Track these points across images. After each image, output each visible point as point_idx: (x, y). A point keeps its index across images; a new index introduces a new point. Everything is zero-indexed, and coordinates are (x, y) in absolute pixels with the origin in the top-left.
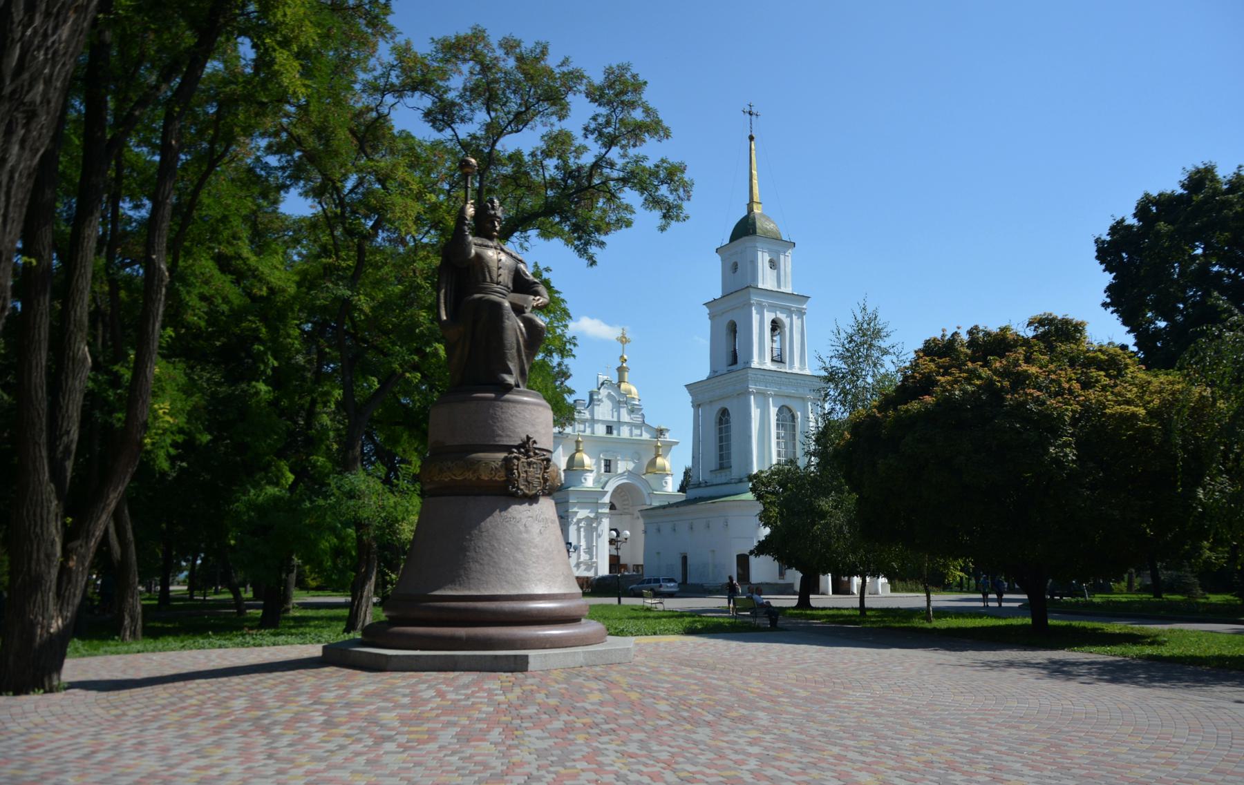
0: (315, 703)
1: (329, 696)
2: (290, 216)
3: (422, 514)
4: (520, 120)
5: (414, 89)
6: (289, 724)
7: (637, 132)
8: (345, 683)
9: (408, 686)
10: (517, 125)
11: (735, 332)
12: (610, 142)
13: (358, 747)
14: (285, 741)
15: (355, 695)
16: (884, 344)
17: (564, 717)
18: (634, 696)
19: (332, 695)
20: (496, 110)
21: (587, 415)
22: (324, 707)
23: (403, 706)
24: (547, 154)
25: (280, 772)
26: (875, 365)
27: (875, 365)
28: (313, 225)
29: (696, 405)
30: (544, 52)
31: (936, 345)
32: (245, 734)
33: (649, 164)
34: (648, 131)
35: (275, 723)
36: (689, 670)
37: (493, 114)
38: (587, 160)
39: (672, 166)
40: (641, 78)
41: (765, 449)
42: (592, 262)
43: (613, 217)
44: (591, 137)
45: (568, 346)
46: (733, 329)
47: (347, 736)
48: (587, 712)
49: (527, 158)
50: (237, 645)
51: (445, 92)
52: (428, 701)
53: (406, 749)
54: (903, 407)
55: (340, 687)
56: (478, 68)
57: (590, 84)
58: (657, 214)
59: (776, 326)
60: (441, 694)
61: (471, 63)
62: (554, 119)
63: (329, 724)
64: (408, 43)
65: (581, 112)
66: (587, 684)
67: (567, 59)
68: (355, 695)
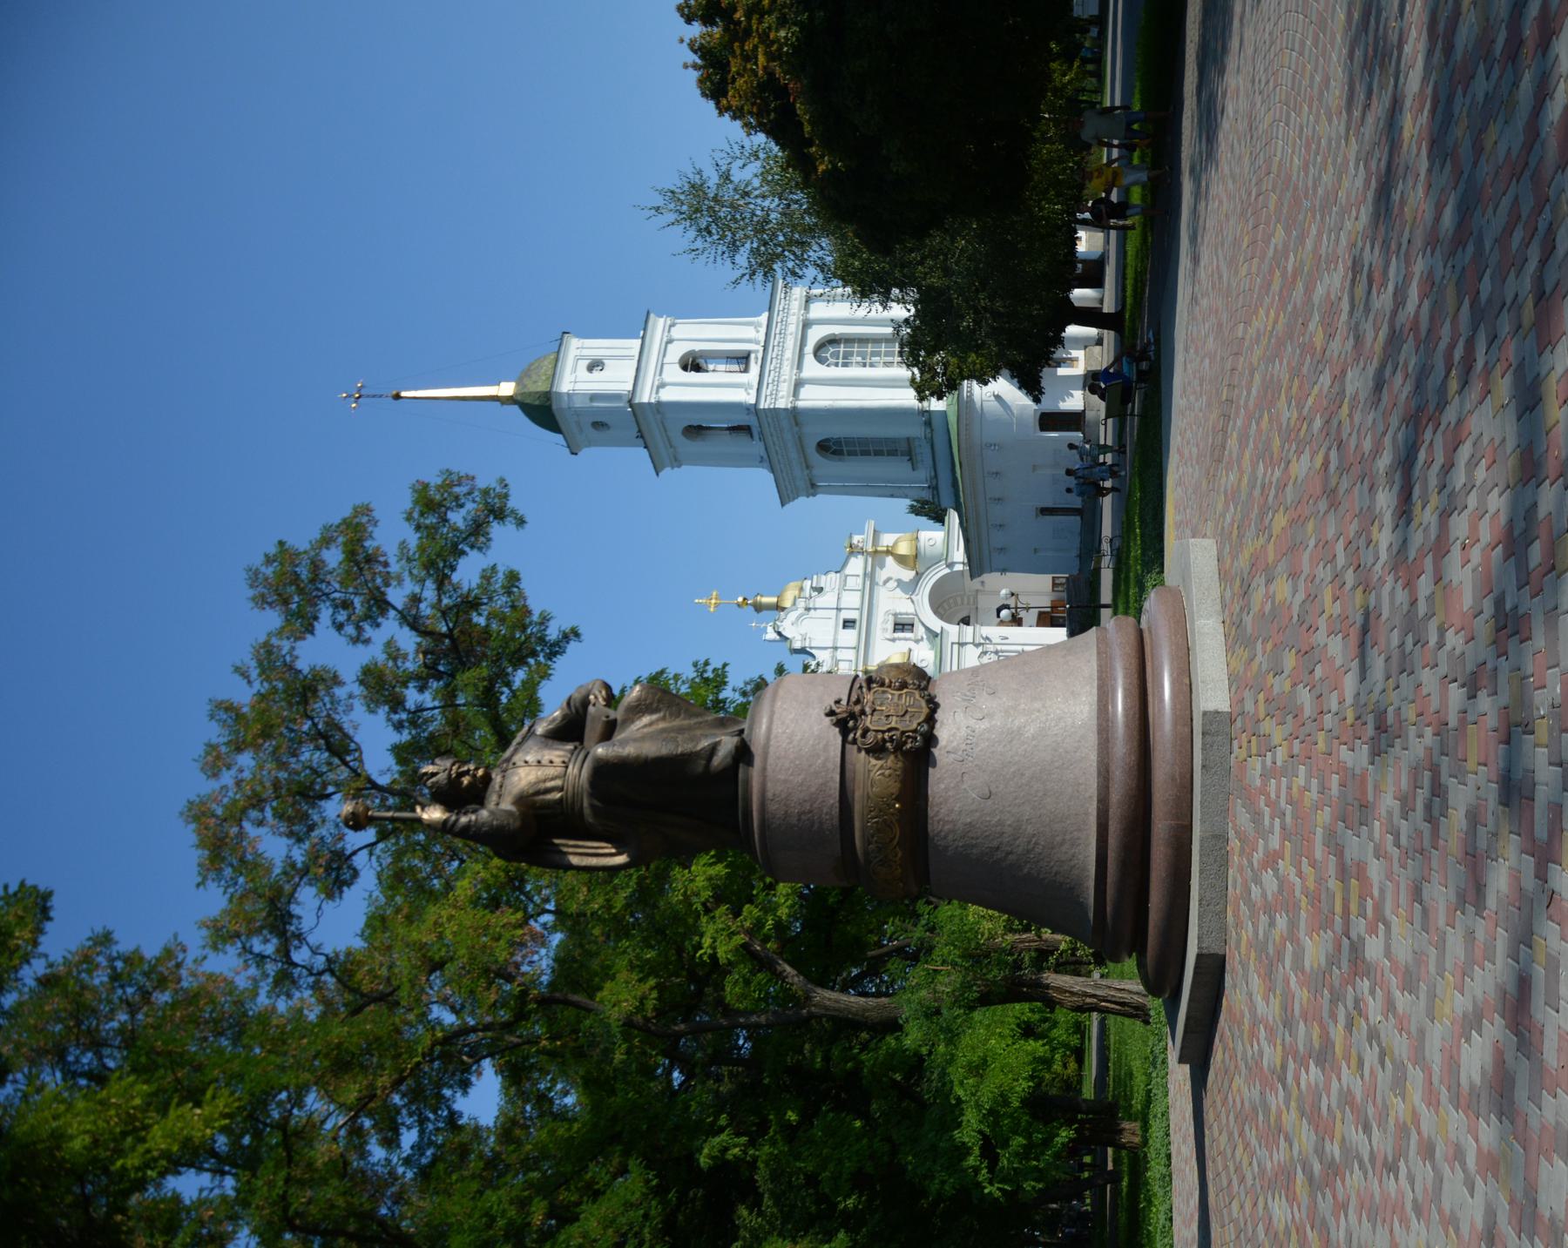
0: (1283, 1080)
1: (1271, 1056)
2: (502, 1112)
3: (967, 898)
4: (338, 745)
5: (287, 917)
6: (1323, 1129)
7: (361, 560)
8: (1246, 1026)
9: (1254, 916)
10: (348, 752)
11: (700, 428)
12: (380, 604)
13: (1374, 1007)
14: (1357, 1137)
15: (1269, 1010)
16: (713, 180)
17: (1320, 637)
18: (1280, 521)
19: (1267, 1050)
20: (325, 785)
22: (1291, 1065)
23: (1293, 925)
24: (397, 703)
25: (1428, 1151)
26: (747, 194)
27: (747, 194)
28: (515, 1075)
29: (813, 488)
30: (229, 708)
31: (709, 77)
32: (1341, 1207)
33: (413, 539)
34: (360, 540)
35: (1320, 1152)
36: (1232, 443)
37: (331, 789)
38: (408, 641)
39: (416, 502)
40: (273, 550)
41: (887, 387)
42: (573, 634)
43: (501, 601)
44: (369, 631)
45: (709, 674)
47: (1350, 1026)
48: (1311, 597)
49: (406, 736)
50: (1167, 1193)
51: (293, 865)
52: (1282, 882)
53: (1380, 916)
54: (807, 128)
55: (1253, 1035)
56: (254, 814)
57: (280, 633)
58: (496, 530)
60: (1271, 860)
61: (247, 825)
62: (340, 692)
63: (1323, 1055)
64: (203, 925)
65: (327, 650)
66: (1255, 608)
67: (237, 670)
68: (1269, 1010)
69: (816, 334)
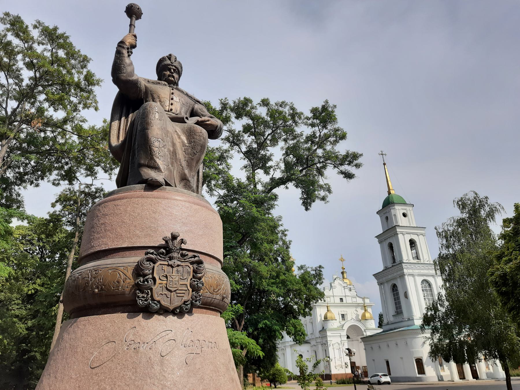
21: (330, 293)
46: (391, 246)
59: (412, 243)
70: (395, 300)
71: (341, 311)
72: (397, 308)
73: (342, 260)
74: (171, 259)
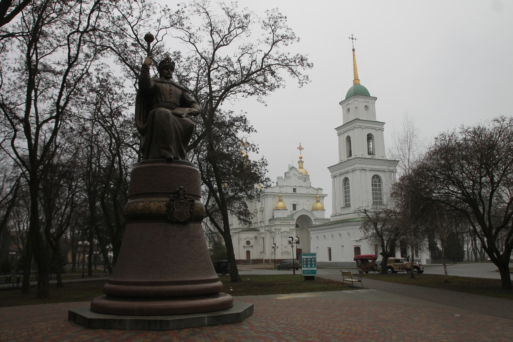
69: (381, 174)
70: (345, 193)
71: (293, 201)
72: (346, 201)
73: (300, 148)
74: (180, 199)
